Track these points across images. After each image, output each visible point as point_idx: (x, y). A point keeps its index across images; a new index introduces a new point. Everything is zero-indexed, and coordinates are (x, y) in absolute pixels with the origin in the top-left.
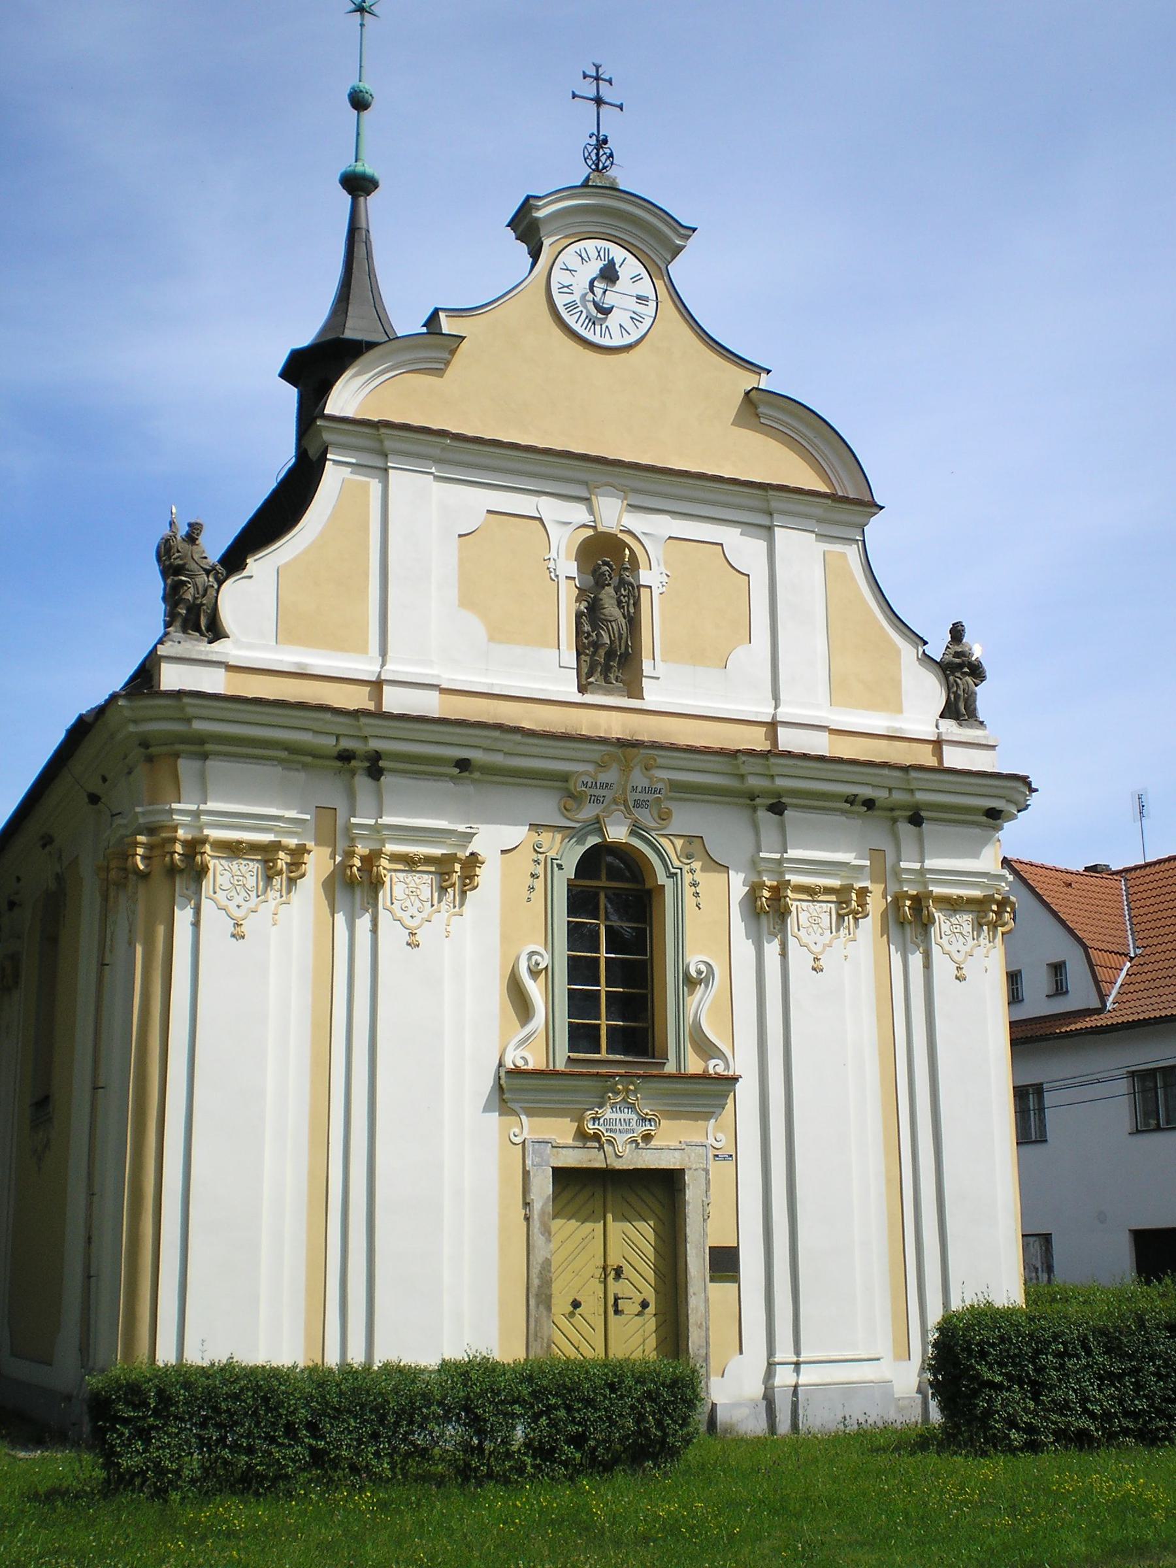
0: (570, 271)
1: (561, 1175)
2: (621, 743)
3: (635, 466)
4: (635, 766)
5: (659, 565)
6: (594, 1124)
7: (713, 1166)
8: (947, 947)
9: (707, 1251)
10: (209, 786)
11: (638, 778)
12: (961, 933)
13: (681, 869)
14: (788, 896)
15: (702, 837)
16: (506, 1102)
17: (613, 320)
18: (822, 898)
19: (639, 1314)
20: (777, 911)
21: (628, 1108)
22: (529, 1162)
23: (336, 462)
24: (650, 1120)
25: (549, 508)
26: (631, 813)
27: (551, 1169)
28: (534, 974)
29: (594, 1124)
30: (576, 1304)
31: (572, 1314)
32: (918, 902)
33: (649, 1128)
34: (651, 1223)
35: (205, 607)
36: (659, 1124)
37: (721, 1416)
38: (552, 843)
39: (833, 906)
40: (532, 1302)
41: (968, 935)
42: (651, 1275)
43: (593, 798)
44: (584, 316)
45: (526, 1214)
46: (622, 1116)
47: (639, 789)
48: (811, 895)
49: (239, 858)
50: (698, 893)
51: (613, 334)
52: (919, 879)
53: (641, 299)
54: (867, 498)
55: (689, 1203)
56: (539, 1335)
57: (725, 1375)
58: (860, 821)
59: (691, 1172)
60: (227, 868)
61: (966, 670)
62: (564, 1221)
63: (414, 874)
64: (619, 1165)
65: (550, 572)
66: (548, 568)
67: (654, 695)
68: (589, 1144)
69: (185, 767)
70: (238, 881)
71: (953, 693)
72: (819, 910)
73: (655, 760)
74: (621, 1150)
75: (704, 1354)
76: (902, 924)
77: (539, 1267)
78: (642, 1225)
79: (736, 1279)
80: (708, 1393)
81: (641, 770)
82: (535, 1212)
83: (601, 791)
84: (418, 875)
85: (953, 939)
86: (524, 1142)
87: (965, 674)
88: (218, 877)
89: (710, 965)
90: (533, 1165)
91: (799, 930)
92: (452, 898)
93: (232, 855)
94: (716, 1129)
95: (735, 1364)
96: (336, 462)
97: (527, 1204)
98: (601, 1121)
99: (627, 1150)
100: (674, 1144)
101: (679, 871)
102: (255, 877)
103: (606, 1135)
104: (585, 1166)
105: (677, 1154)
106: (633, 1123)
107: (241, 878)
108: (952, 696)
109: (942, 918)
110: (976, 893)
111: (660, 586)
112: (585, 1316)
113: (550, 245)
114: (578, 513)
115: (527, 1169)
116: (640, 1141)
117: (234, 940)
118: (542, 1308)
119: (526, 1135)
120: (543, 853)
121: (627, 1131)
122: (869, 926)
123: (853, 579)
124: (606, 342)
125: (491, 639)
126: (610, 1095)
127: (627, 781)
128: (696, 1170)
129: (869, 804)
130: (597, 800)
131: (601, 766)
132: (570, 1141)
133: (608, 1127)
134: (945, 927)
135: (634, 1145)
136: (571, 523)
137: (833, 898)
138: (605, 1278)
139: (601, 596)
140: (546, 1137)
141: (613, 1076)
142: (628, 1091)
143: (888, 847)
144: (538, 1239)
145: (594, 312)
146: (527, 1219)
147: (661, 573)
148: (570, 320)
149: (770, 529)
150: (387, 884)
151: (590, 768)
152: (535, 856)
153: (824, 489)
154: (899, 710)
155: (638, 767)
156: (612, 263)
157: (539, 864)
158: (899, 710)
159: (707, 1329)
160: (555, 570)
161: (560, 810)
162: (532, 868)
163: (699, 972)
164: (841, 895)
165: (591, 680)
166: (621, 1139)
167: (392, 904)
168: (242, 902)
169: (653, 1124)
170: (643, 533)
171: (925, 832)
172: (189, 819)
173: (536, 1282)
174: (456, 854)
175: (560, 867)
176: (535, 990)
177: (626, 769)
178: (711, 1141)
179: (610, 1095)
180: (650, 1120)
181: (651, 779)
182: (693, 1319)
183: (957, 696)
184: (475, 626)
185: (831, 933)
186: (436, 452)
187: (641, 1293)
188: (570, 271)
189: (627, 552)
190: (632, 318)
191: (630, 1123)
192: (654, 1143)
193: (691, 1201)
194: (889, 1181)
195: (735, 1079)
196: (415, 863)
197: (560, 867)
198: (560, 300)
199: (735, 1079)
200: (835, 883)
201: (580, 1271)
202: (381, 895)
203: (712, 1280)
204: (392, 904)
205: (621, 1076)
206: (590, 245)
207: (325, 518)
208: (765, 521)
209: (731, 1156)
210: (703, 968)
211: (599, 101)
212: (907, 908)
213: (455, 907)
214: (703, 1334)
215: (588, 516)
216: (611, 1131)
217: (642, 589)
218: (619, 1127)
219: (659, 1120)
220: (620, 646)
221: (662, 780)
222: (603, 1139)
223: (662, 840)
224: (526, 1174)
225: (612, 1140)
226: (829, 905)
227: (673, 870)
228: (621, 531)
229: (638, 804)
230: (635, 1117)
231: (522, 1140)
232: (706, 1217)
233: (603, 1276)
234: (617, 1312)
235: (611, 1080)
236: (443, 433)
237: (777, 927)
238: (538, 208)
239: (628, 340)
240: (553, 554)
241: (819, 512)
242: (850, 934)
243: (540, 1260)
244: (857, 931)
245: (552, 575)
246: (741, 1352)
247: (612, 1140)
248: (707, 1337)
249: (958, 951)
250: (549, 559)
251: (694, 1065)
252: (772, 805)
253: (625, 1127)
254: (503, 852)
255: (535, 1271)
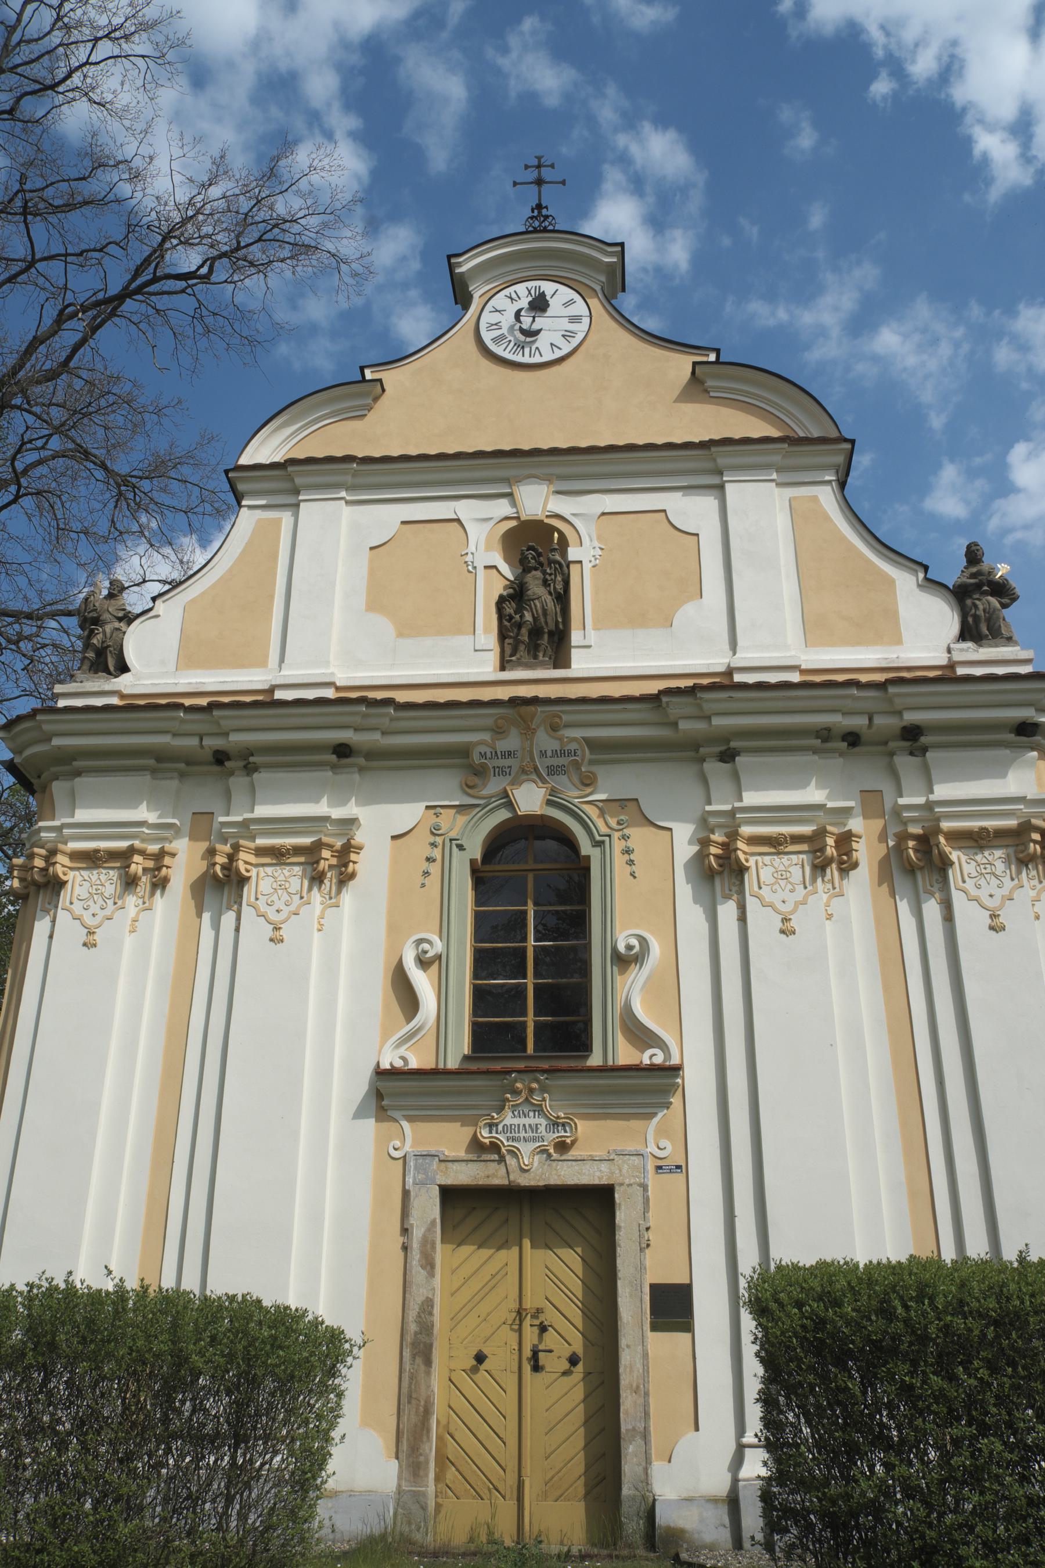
0: (497, 311)
1: (450, 1195)
2: (515, 702)
3: (554, 451)
4: (538, 727)
5: (591, 541)
6: (491, 1132)
7: (652, 1179)
8: (973, 892)
9: (647, 1290)
10: (77, 802)
11: (544, 740)
12: (994, 874)
13: (609, 836)
14: (738, 849)
15: (637, 800)
16: (386, 1110)
17: (543, 342)
18: (791, 848)
19: (565, 1373)
20: (732, 871)
21: (535, 1111)
22: (410, 1180)
23: (250, 507)
24: (563, 1125)
25: (465, 509)
26: (544, 781)
27: (437, 1188)
28: (423, 963)
29: (491, 1132)
30: (480, 1358)
31: (474, 1370)
32: (926, 842)
33: (563, 1134)
34: (579, 1250)
35: (111, 649)
36: (576, 1129)
37: (664, 1517)
38: (453, 824)
39: (804, 856)
40: (407, 1354)
41: (1004, 874)
42: (578, 1320)
43: (497, 770)
44: (512, 344)
45: (404, 1243)
46: (526, 1121)
47: (549, 753)
48: (775, 847)
49: (98, 867)
50: (632, 861)
51: (544, 349)
52: (925, 814)
53: (575, 319)
54: (834, 434)
55: (620, 1227)
56: (414, 1395)
57: (673, 1460)
58: (841, 760)
59: (622, 1188)
60: (86, 878)
61: (986, 588)
62: (492, 1251)
63: (283, 867)
64: (524, 1181)
65: (468, 566)
66: (466, 562)
67: (581, 664)
68: (485, 1157)
69: (58, 788)
70: (96, 890)
71: (972, 615)
72: (787, 863)
73: (560, 718)
74: (526, 1163)
75: (642, 1429)
76: (910, 870)
77: (417, 1308)
78: (567, 1253)
79: (687, 1326)
80: (648, 1484)
81: (547, 733)
82: (415, 1240)
83: (504, 760)
84: (288, 868)
85: (982, 882)
86: (405, 1156)
87: (986, 593)
88: (77, 887)
89: (644, 939)
90: (415, 1183)
91: (760, 888)
92: (328, 889)
93: (92, 865)
94: (661, 1132)
95: (687, 1444)
96: (250, 507)
97: (405, 1231)
98: (500, 1127)
99: (536, 1164)
100: (598, 1153)
101: (607, 839)
102: (114, 885)
103: (506, 1144)
104: (480, 1183)
105: (604, 1167)
106: (542, 1129)
107: (99, 887)
108: (970, 620)
109: (963, 858)
110: (1012, 823)
111: (593, 559)
112: (493, 1373)
113: (480, 297)
114: (502, 508)
115: (407, 1187)
116: (552, 1151)
117: (85, 948)
118: (419, 1361)
119: (408, 1148)
120: (442, 835)
121: (534, 1140)
122: (864, 875)
123: (827, 518)
124: (537, 359)
125: (400, 635)
126: (509, 1096)
127: (532, 745)
128: (630, 1185)
129: (853, 739)
130: (502, 771)
131: (499, 732)
132: (462, 1154)
133: (508, 1134)
134: (969, 868)
135: (545, 1156)
136: (492, 518)
137: (805, 847)
138: (520, 1325)
139: (526, 580)
140: (432, 1150)
141: (509, 1072)
142: (531, 1091)
143: (887, 788)
144: (418, 1274)
145: (522, 338)
146: (405, 1248)
147: (594, 548)
148: (498, 350)
149: (721, 487)
150: (254, 880)
151: (486, 736)
152: (432, 839)
153: (775, 433)
154: (899, 641)
155: (542, 728)
156: (542, 295)
157: (436, 846)
158: (899, 641)
159: (647, 1394)
160: (472, 562)
161: (461, 787)
162: (428, 851)
163: (630, 947)
164: (814, 842)
165: (514, 658)
166: (526, 1149)
167: (257, 899)
168: (98, 911)
169: (568, 1129)
170: (573, 515)
171: (929, 761)
172: (54, 835)
173: (413, 1327)
174: (320, 839)
175: (461, 847)
176: (423, 983)
177: (528, 731)
178: (652, 1148)
179: (509, 1096)
180: (563, 1125)
181: (560, 739)
182: (625, 1380)
183: (976, 618)
184: (383, 626)
185: (805, 888)
186: (349, 479)
187: (569, 1344)
188: (499, 311)
189: (556, 535)
190: (563, 336)
191: (537, 1129)
192: (573, 1153)
193: (623, 1225)
194: (913, 1195)
195: (677, 1069)
196: (283, 855)
197: (461, 847)
198: (487, 337)
199: (677, 1069)
200: (806, 829)
201: (488, 1314)
202: (246, 889)
203: (654, 1328)
204: (257, 899)
205: (519, 1071)
206: (521, 288)
207: (236, 555)
208: (714, 480)
209: (679, 1167)
210: (634, 942)
211: (539, 182)
212: (911, 852)
213: (331, 898)
214: (641, 1401)
215: (510, 508)
216: (514, 1139)
217: (572, 566)
218: (522, 1134)
219: (576, 1124)
220: (546, 623)
221: (575, 739)
222: (503, 1150)
223: (585, 807)
224: (406, 1194)
225: (515, 1150)
226: (801, 856)
227: (598, 838)
228: (547, 516)
229: (552, 771)
230: (543, 1122)
231: (402, 1155)
232: (644, 1245)
233: (517, 1322)
234: (537, 1368)
235: (508, 1077)
236: (349, 459)
237: (734, 889)
238: (459, 265)
239: (559, 354)
240: (472, 548)
241: (776, 459)
242: (834, 888)
243: (420, 1300)
244: (845, 882)
245: (470, 568)
246: (697, 1429)
247: (515, 1150)
248: (646, 1406)
249: (991, 896)
250: (467, 554)
251: (625, 1054)
252: (721, 752)
253: (531, 1134)
254: (394, 838)
255: (412, 1315)
